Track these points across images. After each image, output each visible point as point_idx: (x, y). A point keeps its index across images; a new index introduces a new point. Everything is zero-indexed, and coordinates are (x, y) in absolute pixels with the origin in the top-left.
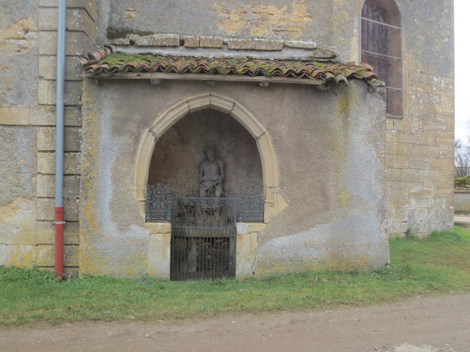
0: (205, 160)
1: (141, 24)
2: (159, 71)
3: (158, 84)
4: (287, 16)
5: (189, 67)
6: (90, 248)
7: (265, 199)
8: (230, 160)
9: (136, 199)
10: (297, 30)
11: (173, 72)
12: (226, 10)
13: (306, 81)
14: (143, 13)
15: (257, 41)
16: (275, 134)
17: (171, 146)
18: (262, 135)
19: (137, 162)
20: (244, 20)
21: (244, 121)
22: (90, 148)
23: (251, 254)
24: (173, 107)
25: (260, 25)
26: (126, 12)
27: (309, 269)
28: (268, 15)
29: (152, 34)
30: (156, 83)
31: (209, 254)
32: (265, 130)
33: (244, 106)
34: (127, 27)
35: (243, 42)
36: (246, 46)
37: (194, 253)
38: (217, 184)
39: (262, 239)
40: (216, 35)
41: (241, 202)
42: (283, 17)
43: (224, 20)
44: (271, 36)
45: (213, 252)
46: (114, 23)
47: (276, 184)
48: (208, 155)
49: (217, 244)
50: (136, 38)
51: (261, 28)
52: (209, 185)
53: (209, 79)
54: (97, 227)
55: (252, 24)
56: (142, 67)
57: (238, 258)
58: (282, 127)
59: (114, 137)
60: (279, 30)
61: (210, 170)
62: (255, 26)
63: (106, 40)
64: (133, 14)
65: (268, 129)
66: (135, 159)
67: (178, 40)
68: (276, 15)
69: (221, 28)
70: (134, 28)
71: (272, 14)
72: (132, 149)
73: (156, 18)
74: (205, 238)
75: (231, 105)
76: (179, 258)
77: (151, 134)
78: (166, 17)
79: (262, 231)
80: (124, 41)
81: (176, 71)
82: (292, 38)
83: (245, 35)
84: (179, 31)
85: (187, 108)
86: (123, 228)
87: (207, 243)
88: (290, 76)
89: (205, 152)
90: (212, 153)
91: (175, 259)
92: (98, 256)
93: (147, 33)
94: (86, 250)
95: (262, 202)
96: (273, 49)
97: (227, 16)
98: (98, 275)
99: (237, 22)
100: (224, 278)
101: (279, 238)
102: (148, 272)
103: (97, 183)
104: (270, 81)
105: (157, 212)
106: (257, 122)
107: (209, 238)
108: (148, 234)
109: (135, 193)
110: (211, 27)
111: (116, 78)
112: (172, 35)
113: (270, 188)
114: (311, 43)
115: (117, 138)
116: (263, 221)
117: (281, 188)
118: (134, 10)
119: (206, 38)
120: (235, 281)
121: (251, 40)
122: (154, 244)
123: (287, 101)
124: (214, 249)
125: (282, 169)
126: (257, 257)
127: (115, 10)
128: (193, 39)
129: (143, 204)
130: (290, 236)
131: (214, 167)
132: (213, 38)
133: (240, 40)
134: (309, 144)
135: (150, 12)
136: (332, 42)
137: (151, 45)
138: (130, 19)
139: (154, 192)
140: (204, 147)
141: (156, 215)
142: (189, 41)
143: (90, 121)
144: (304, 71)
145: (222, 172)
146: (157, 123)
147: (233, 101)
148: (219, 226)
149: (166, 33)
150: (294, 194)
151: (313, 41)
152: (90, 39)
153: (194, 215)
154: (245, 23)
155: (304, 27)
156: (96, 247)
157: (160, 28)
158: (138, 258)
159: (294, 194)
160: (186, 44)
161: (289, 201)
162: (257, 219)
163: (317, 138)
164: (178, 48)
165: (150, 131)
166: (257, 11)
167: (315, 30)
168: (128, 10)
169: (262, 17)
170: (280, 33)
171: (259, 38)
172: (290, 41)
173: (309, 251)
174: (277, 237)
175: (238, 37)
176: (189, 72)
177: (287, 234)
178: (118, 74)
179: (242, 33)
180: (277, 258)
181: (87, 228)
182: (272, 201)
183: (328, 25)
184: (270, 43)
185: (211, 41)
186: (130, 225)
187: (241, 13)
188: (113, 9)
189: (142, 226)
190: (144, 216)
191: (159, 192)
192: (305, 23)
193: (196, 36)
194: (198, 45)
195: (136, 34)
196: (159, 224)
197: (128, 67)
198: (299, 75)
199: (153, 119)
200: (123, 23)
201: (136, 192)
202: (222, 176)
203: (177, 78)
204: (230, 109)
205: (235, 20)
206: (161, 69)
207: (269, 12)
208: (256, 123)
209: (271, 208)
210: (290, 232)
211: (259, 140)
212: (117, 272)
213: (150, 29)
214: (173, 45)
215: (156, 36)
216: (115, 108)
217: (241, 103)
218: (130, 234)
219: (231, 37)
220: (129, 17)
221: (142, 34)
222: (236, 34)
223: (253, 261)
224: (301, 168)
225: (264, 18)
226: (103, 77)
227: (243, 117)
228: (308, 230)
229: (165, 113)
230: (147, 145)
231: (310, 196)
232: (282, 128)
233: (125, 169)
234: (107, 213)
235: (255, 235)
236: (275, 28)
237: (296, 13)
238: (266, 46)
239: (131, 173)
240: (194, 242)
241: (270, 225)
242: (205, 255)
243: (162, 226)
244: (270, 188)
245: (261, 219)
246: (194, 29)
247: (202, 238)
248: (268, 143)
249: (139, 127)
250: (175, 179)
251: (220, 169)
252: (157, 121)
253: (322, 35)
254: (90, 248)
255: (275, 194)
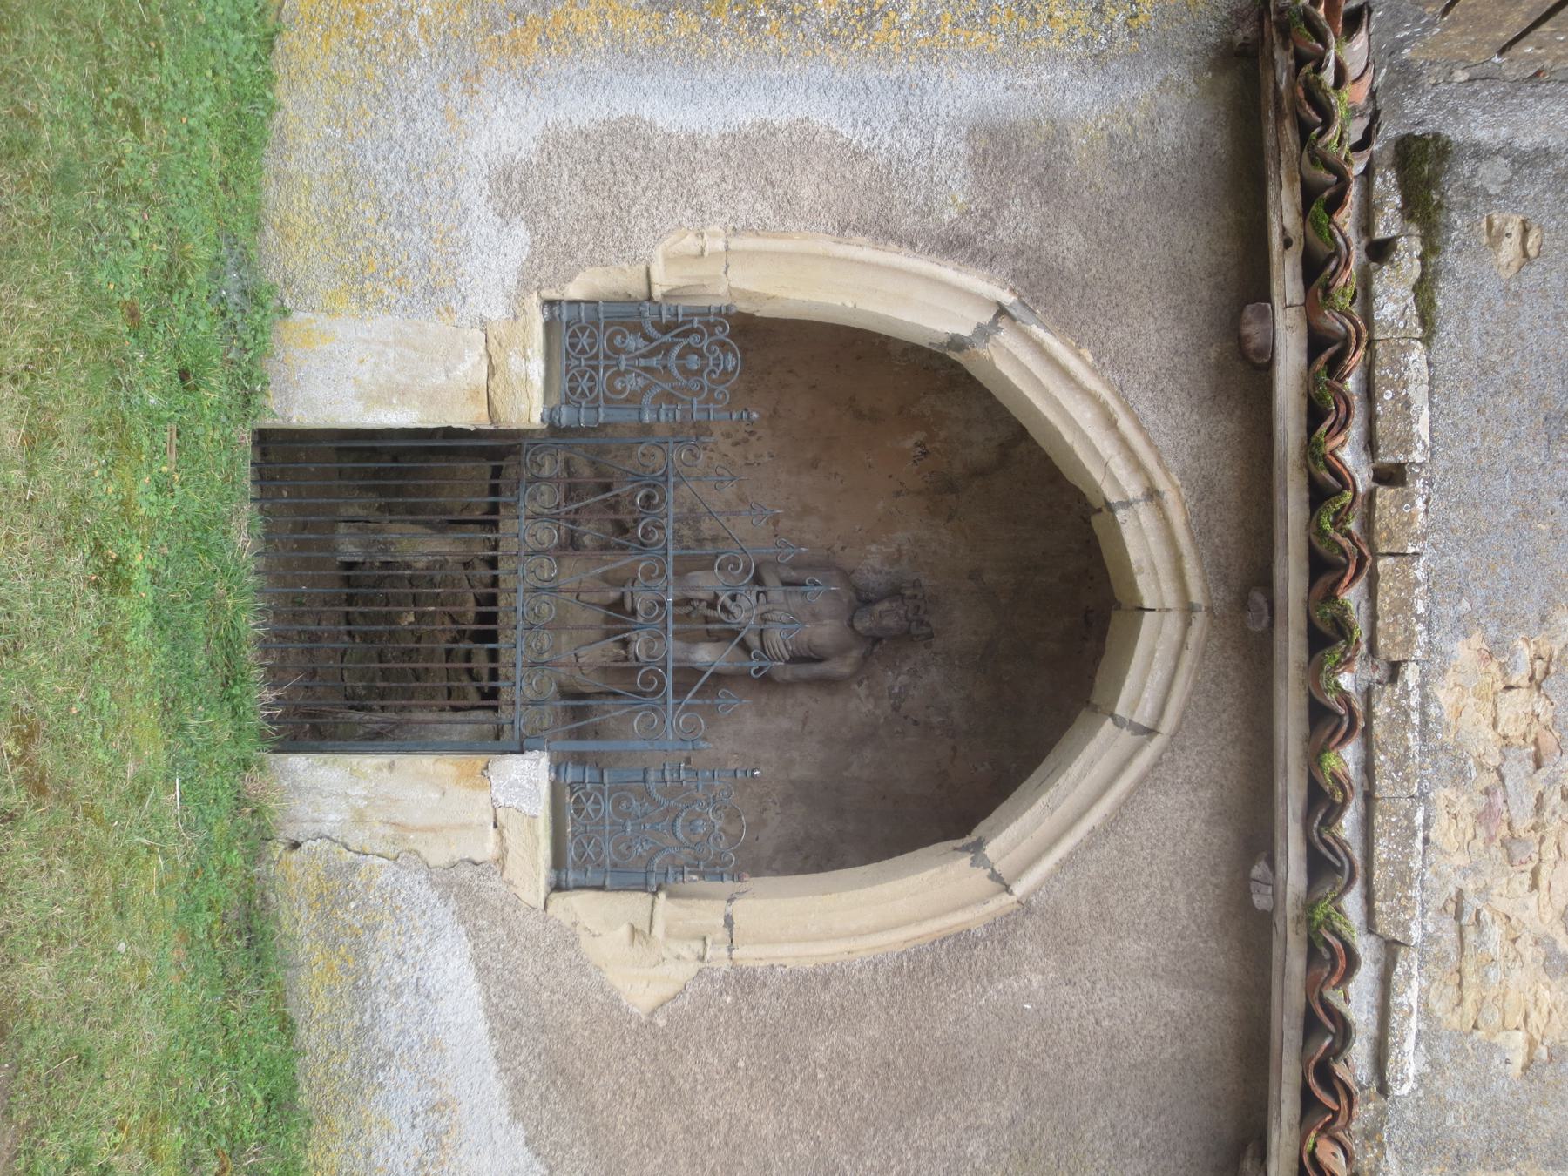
0: (857, 591)
1: (1468, 288)
2: (1317, 342)
3: (1241, 340)
4: (1528, 953)
5: (1349, 494)
6: (414, 30)
7: (670, 896)
8: (860, 705)
9: (658, 254)
10: (1469, 1004)
11: (1315, 414)
12: (1547, 673)
13: (1287, 1107)
14: (1517, 295)
15: (1411, 821)
16: (1003, 942)
17: (920, 436)
18: (995, 876)
19: (842, 250)
20: (1505, 758)
21: (1063, 782)
22: (907, 16)
23: (389, 831)
24: (1125, 424)
25: (1482, 832)
26: (1518, 219)
27: (317, 1128)
28: (1530, 866)
29: (1427, 340)
30: (1252, 330)
31: (419, 618)
32: (1020, 889)
33: (1142, 780)
34: (1449, 227)
35: (1406, 756)
36: (1389, 767)
37: (422, 548)
38: (744, 647)
39: (464, 887)
40: (1429, 629)
41: (652, 776)
42: (1527, 939)
43: (1502, 666)
44: (1436, 884)
45: (432, 635)
46: (1466, 169)
47: (749, 955)
48: (885, 605)
49: (468, 656)
50: (1406, 264)
51: (1469, 835)
52: (745, 612)
53: (1279, 603)
54: (514, 62)
55: (1487, 792)
56: (1337, 253)
57: (370, 763)
58: (1036, 980)
59: (964, 131)
60: (1465, 920)
61: (815, 617)
62: (1480, 808)
63: (1392, 134)
64: (1509, 250)
65: (1025, 906)
66: (859, 238)
67: (1402, 459)
68: (1532, 902)
69: (1465, 652)
70: (1449, 258)
71: (1534, 886)
72: (908, 223)
73: (1495, 357)
74: (493, 600)
75: (1144, 716)
76: (401, 474)
77: (986, 318)
78: (1502, 399)
79: (509, 883)
80: (1389, 212)
81: (1323, 428)
82: (1431, 979)
83: (1433, 764)
84: (1441, 463)
85: (1123, 492)
86: (516, 189)
87: (471, 609)
88: (1311, 1026)
89: (895, 593)
90: (888, 624)
91: (396, 455)
92: (369, 69)
93: (1426, 317)
94: (400, 11)
95: (653, 881)
96: (1380, 894)
97: (1520, 676)
98: (280, 71)
99: (1495, 725)
100: (270, 696)
101: (472, 973)
102: (297, 316)
103: (735, 56)
104: (1278, 918)
105: (596, 356)
106: (1060, 852)
107: (492, 618)
108: (487, 313)
109: (690, 243)
110: (1465, 605)
111: (1270, 128)
112: (1422, 428)
113: (729, 922)
114: (1411, 1071)
115: (961, 147)
116: (557, 887)
117: (725, 977)
118: (1526, 255)
119: (1417, 583)
120: (249, 748)
121: (1415, 791)
122: (423, 341)
123: (1175, 1000)
124: (443, 645)
125: (826, 983)
126: (377, 861)
127: (1526, 171)
128: (1409, 523)
129: (637, 288)
130: (482, 1028)
131: (825, 632)
132: (1418, 617)
133: (1412, 739)
134: (955, 1116)
135: (1524, 326)
136: (1419, 1166)
137: (1377, 336)
138: (1485, 240)
139: (693, 340)
140: (916, 584)
141: (583, 351)
142: (1399, 507)
143: (1042, 17)
144: (1344, 1102)
145: (804, 671)
146: (1039, 348)
147: (1167, 726)
148: (534, 665)
149: (1432, 405)
150: (699, 1045)
151: (1420, 1079)
152: (1431, 24)
153: (605, 547)
154: (1494, 761)
155: (1480, 1034)
156: (417, 58)
157: (1451, 372)
158: (364, 267)
159: (699, 1045)
160: (1385, 495)
161: (661, 1022)
162: (571, 854)
163: (987, 1160)
164: (1364, 457)
165: (1002, 311)
166: (1547, 815)
167: (1471, 1087)
168: (1525, 232)
169: (1520, 840)
170: (1448, 923)
171: (1427, 826)
172: (1415, 971)
173: (406, 1126)
174: (475, 959)
175: (1425, 732)
176: (1319, 495)
177: (493, 1013)
178: (1289, 133)
179: (1443, 748)
180: (373, 962)
181: (507, 11)
182: (658, 930)
183: (1495, 1146)
184: (1404, 878)
185: (1405, 606)
186: (530, 222)
187: (1536, 742)
188: (1526, 161)
189: (524, 285)
190: (574, 291)
191: (693, 362)
192: (1499, 1039)
193: (1425, 536)
194: (1384, 550)
195: (1423, 266)
196: (536, 369)
197: (1333, 179)
198: (1325, 1074)
199: (1064, 326)
200: (1468, 206)
201: (695, 250)
202: (786, 672)
203: (1279, 436)
204: (1120, 709)
205: (1504, 716)
206: (1331, 351)
207: (1545, 870)
208: (1055, 840)
209: (624, 930)
210: (503, 1024)
211: (966, 860)
212: (293, 167)
213: (1447, 329)
214: (1380, 432)
215: (1417, 354)
216: (1111, 137)
217: (1157, 764)
218: (482, 222)
219: (1425, 698)
220: (1496, 237)
221: (1423, 289)
222: (1438, 720)
223: (357, 838)
224: (832, 1079)
225: (1516, 849)
226: (1273, 63)
227: (1082, 776)
228: (516, 1116)
229: (1093, 384)
230: (929, 301)
231: (687, 1130)
232: (1031, 981)
233: (807, 191)
234: (583, 110)
235: (488, 849)
236: (1472, 902)
237: (1546, 997)
238: (1388, 862)
239: (789, 223)
240: (474, 543)
241: (540, 927)
242: (416, 600)
243: (526, 380)
244: (729, 922)
245: (571, 877)
246: (1454, 530)
247: (495, 582)
248: (955, 909)
249: (1019, 253)
250: (767, 459)
251: (820, 660)
252: (1054, 344)
253: (1450, 1122)
254: (414, 30)
255: (698, 946)
